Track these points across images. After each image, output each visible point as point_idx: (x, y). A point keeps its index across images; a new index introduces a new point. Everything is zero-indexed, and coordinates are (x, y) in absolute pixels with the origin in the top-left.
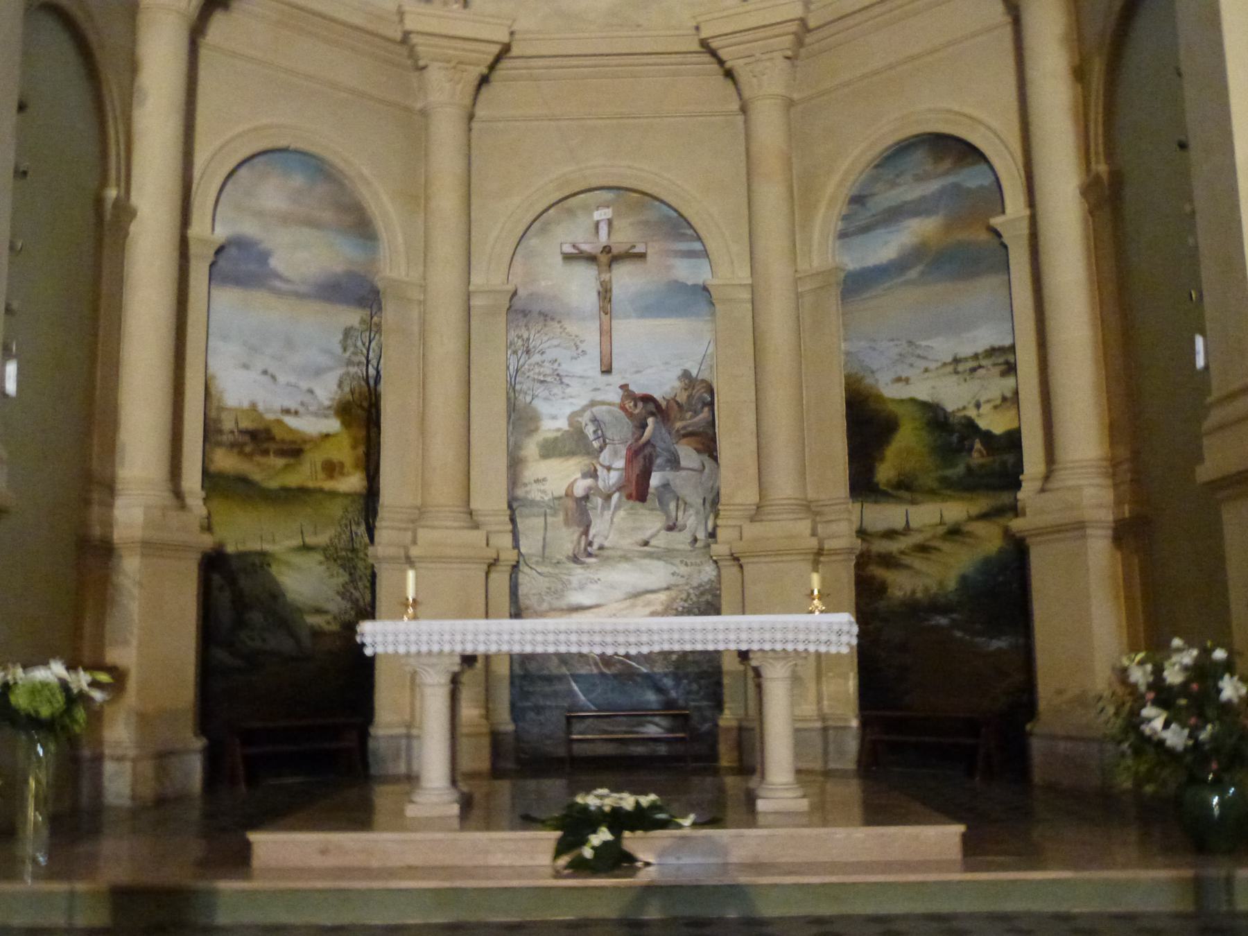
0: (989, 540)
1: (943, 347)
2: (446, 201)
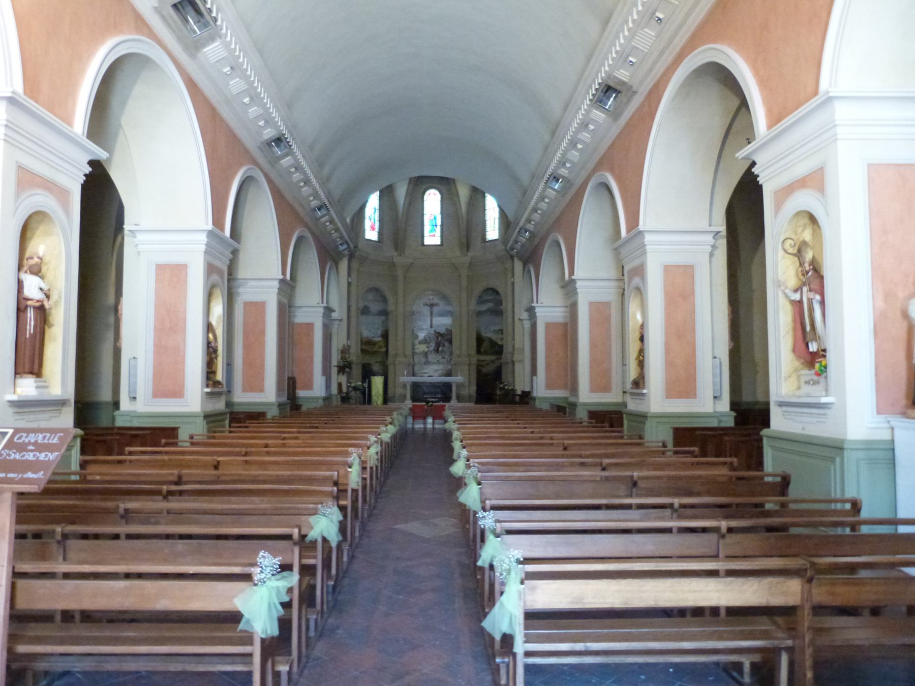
0: (497, 364)
1: (493, 328)
2: (400, 294)
